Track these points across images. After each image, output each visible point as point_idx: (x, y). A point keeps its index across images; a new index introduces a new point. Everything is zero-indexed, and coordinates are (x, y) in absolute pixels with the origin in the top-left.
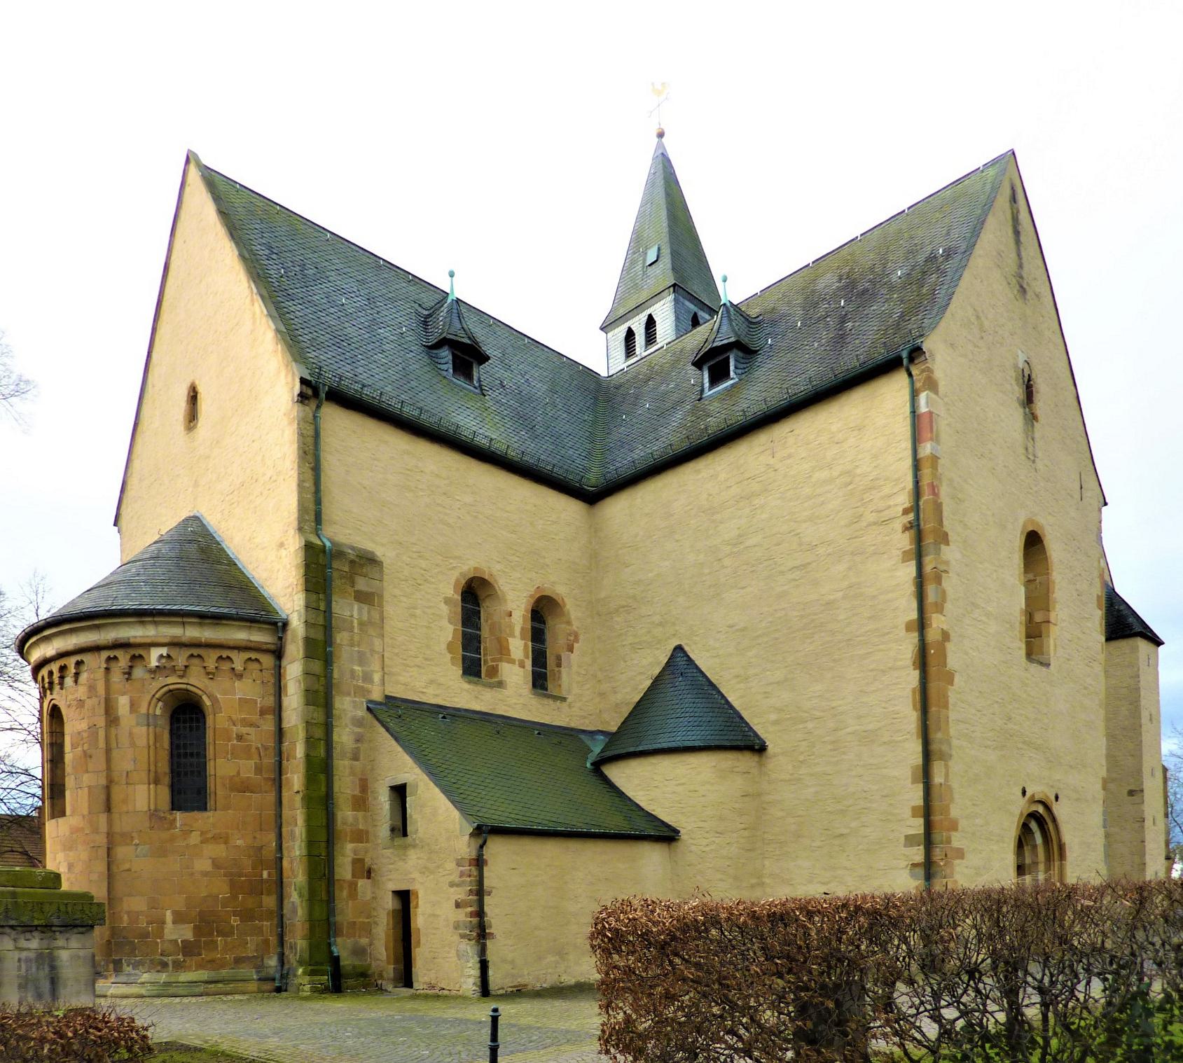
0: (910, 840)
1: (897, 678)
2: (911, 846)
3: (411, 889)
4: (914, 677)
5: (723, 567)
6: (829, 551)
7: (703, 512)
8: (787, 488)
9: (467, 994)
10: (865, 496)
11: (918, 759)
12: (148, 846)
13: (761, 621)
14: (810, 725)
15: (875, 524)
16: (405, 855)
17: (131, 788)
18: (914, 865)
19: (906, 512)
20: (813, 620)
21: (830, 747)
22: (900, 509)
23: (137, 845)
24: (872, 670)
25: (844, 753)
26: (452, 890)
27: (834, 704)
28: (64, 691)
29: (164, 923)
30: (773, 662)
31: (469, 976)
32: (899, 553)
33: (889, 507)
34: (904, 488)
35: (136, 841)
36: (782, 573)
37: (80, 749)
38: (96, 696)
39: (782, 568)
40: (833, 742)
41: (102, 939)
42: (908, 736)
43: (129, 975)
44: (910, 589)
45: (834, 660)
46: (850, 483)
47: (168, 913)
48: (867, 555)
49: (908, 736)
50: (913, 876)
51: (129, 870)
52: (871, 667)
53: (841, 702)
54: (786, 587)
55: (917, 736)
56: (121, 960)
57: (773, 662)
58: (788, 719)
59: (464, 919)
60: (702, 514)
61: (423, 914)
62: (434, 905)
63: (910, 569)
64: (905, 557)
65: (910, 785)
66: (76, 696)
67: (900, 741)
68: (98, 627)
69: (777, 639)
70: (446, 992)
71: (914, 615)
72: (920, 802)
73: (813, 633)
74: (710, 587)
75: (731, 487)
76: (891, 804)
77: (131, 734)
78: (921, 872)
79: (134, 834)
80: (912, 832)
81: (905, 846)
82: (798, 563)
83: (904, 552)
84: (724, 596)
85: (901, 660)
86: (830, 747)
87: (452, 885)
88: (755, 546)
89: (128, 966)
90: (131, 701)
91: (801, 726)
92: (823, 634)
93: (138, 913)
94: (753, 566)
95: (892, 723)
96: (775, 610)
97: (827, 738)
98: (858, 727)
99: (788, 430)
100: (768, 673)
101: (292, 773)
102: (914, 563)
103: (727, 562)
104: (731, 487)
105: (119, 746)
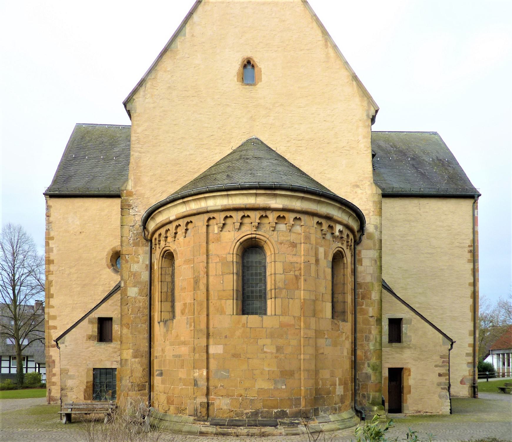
0: (468, 355)
1: (465, 300)
2: (468, 356)
3: (404, 367)
4: (471, 301)
5: (396, 244)
6: (442, 251)
7: (388, 220)
8: (426, 223)
9: (445, 414)
10: (455, 236)
11: (472, 328)
12: (331, 340)
13: (414, 269)
14: (433, 311)
15: (458, 247)
16: (402, 352)
17: (324, 303)
18: (468, 363)
19: (469, 246)
20: (435, 274)
21: (440, 320)
22: (468, 245)
23: (326, 339)
24: (456, 296)
25: (445, 323)
26: (437, 369)
27: (442, 305)
28: (275, 232)
29: (336, 385)
30: (418, 285)
31: (447, 406)
32: (467, 259)
33: (464, 243)
34: (469, 238)
35: (326, 336)
36: (422, 253)
37: (292, 273)
38: (310, 244)
39: (423, 252)
40: (441, 318)
41: (311, 396)
42: (468, 320)
43: (323, 417)
44: (470, 272)
45: (442, 290)
46: (450, 230)
47: (337, 379)
48: (455, 256)
49: (468, 320)
50: (468, 366)
51: (323, 353)
52: (456, 295)
53: (445, 305)
54: (424, 259)
55: (471, 320)
56: (318, 408)
57: (418, 285)
58: (424, 307)
59: (445, 381)
60: (387, 220)
61: (414, 379)
62: (423, 375)
63: (471, 266)
64: (469, 261)
65: (468, 336)
66: (289, 238)
67: (465, 322)
68: (319, 202)
69: (420, 277)
70: (428, 414)
71: (472, 281)
72: (472, 342)
73: (435, 278)
74: (390, 250)
75: (401, 214)
76: (462, 342)
77: (324, 271)
78: (472, 365)
79: (325, 332)
80: (468, 352)
81: (466, 356)
82: (429, 252)
83: (468, 259)
84: (396, 255)
85: (466, 295)
86: (440, 320)
87: (436, 366)
88: (411, 240)
89: (322, 412)
90: (325, 252)
91: (429, 311)
92: (439, 280)
93: (327, 379)
94: (410, 247)
95: (463, 315)
96: (420, 266)
97: (439, 317)
98: (451, 314)
99: (426, 203)
100: (416, 289)
101: (367, 305)
102: (472, 264)
103: (398, 242)
104: (401, 214)
105: (319, 277)
